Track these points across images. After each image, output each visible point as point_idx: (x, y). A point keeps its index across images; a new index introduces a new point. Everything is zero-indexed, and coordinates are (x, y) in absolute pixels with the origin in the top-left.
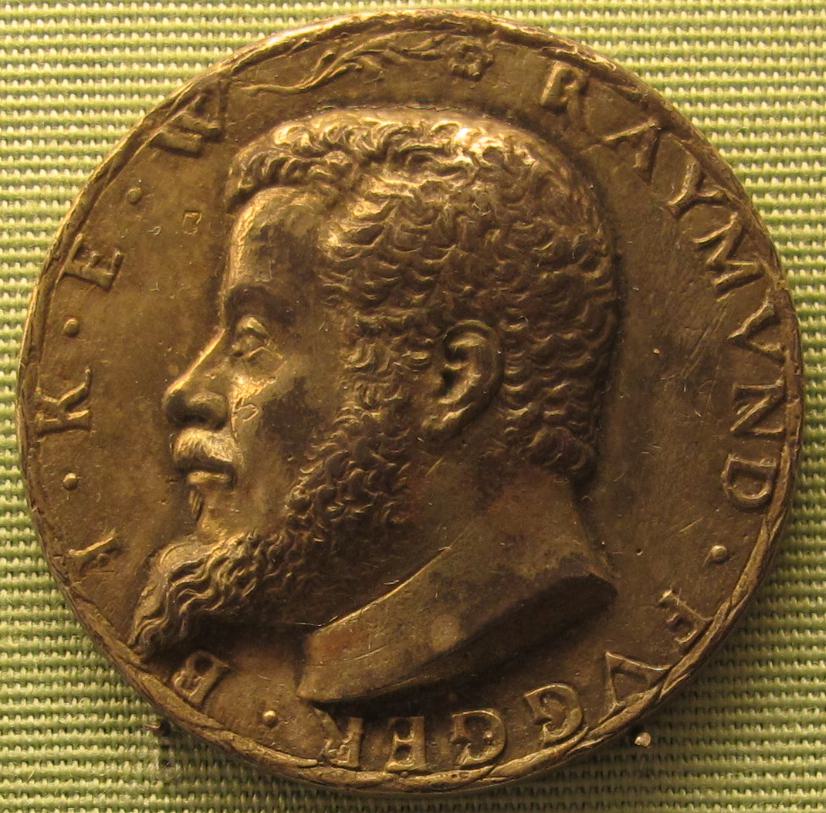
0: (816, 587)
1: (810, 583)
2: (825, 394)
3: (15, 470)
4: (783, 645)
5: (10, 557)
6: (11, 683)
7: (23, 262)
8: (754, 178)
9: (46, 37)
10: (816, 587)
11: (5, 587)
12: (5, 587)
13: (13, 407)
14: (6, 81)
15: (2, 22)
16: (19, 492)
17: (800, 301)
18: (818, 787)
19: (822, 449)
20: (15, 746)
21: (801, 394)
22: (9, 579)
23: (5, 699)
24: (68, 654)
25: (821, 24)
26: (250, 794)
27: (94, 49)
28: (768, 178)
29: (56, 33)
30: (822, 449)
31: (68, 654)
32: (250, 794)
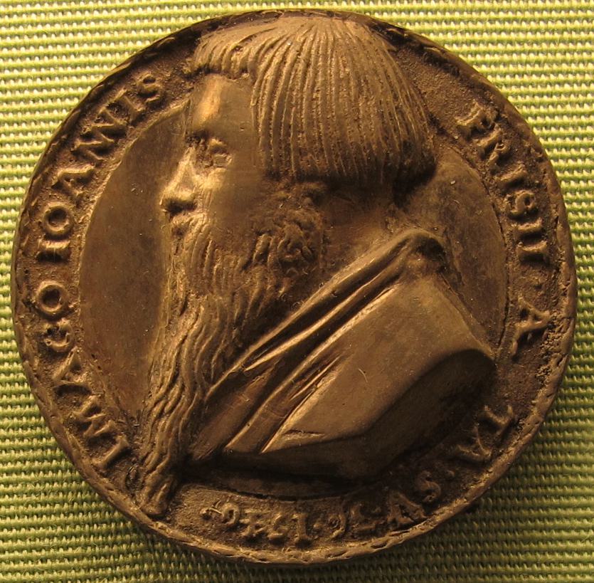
0: (585, 434)
1: (583, 398)
2: (593, 298)
3: (10, 333)
4: (565, 419)
5: (7, 484)
6: (8, 505)
7: (15, 187)
8: (535, 117)
9: (37, 113)
10: (586, 380)
11: (2, 427)
12: (2, 427)
13: (18, 354)
14: (4, 60)
15: (1, 114)
16: (10, 249)
17: (580, 255)
18: (589, 518)
19: (591, 370)
20: (5, 440)
21: (574, 295)
22: (6, 421)
23: (4, 516)
24: (48, 505)
25: (590, 157)
26: (220, 572)
27: (18, 124)
28: (554, 137)
29: (37, 24)
30: (591, 370)
31: (48, 505)
32: (220, 572)
